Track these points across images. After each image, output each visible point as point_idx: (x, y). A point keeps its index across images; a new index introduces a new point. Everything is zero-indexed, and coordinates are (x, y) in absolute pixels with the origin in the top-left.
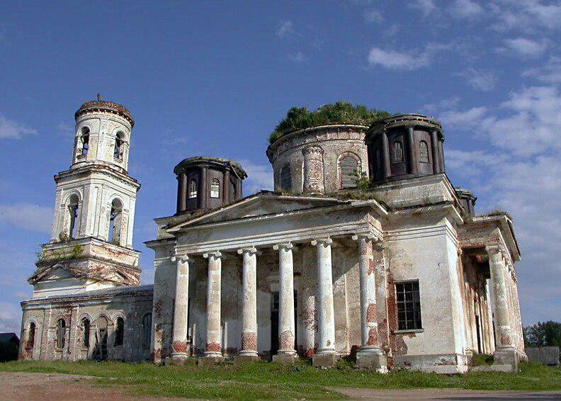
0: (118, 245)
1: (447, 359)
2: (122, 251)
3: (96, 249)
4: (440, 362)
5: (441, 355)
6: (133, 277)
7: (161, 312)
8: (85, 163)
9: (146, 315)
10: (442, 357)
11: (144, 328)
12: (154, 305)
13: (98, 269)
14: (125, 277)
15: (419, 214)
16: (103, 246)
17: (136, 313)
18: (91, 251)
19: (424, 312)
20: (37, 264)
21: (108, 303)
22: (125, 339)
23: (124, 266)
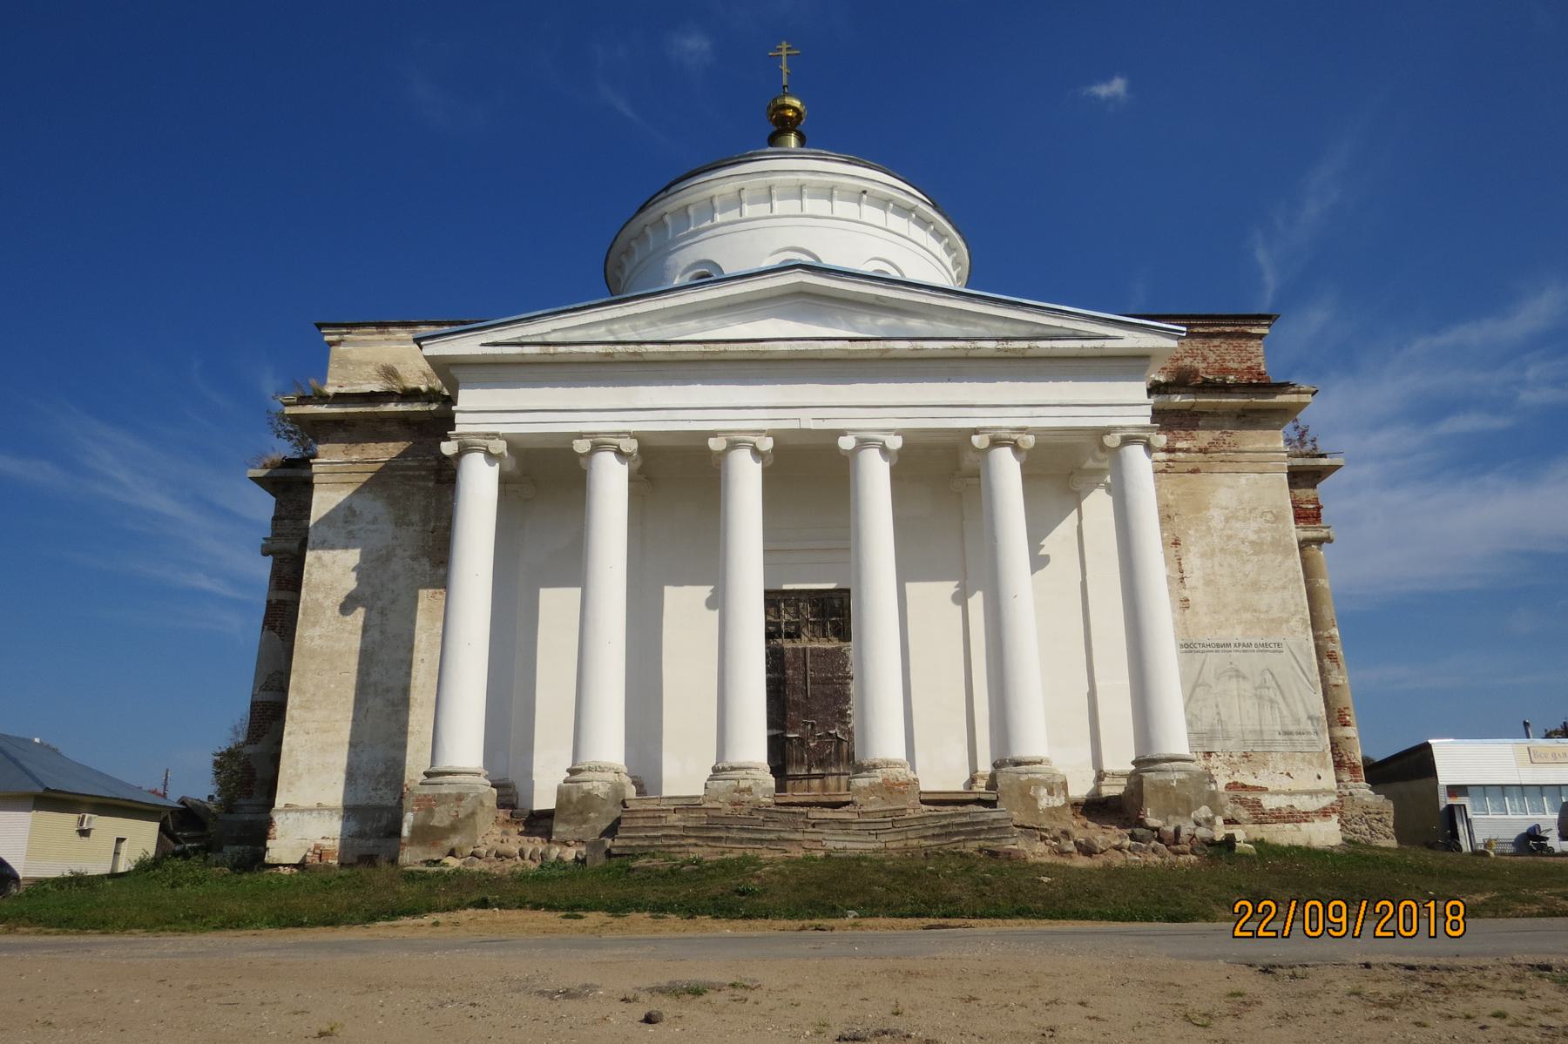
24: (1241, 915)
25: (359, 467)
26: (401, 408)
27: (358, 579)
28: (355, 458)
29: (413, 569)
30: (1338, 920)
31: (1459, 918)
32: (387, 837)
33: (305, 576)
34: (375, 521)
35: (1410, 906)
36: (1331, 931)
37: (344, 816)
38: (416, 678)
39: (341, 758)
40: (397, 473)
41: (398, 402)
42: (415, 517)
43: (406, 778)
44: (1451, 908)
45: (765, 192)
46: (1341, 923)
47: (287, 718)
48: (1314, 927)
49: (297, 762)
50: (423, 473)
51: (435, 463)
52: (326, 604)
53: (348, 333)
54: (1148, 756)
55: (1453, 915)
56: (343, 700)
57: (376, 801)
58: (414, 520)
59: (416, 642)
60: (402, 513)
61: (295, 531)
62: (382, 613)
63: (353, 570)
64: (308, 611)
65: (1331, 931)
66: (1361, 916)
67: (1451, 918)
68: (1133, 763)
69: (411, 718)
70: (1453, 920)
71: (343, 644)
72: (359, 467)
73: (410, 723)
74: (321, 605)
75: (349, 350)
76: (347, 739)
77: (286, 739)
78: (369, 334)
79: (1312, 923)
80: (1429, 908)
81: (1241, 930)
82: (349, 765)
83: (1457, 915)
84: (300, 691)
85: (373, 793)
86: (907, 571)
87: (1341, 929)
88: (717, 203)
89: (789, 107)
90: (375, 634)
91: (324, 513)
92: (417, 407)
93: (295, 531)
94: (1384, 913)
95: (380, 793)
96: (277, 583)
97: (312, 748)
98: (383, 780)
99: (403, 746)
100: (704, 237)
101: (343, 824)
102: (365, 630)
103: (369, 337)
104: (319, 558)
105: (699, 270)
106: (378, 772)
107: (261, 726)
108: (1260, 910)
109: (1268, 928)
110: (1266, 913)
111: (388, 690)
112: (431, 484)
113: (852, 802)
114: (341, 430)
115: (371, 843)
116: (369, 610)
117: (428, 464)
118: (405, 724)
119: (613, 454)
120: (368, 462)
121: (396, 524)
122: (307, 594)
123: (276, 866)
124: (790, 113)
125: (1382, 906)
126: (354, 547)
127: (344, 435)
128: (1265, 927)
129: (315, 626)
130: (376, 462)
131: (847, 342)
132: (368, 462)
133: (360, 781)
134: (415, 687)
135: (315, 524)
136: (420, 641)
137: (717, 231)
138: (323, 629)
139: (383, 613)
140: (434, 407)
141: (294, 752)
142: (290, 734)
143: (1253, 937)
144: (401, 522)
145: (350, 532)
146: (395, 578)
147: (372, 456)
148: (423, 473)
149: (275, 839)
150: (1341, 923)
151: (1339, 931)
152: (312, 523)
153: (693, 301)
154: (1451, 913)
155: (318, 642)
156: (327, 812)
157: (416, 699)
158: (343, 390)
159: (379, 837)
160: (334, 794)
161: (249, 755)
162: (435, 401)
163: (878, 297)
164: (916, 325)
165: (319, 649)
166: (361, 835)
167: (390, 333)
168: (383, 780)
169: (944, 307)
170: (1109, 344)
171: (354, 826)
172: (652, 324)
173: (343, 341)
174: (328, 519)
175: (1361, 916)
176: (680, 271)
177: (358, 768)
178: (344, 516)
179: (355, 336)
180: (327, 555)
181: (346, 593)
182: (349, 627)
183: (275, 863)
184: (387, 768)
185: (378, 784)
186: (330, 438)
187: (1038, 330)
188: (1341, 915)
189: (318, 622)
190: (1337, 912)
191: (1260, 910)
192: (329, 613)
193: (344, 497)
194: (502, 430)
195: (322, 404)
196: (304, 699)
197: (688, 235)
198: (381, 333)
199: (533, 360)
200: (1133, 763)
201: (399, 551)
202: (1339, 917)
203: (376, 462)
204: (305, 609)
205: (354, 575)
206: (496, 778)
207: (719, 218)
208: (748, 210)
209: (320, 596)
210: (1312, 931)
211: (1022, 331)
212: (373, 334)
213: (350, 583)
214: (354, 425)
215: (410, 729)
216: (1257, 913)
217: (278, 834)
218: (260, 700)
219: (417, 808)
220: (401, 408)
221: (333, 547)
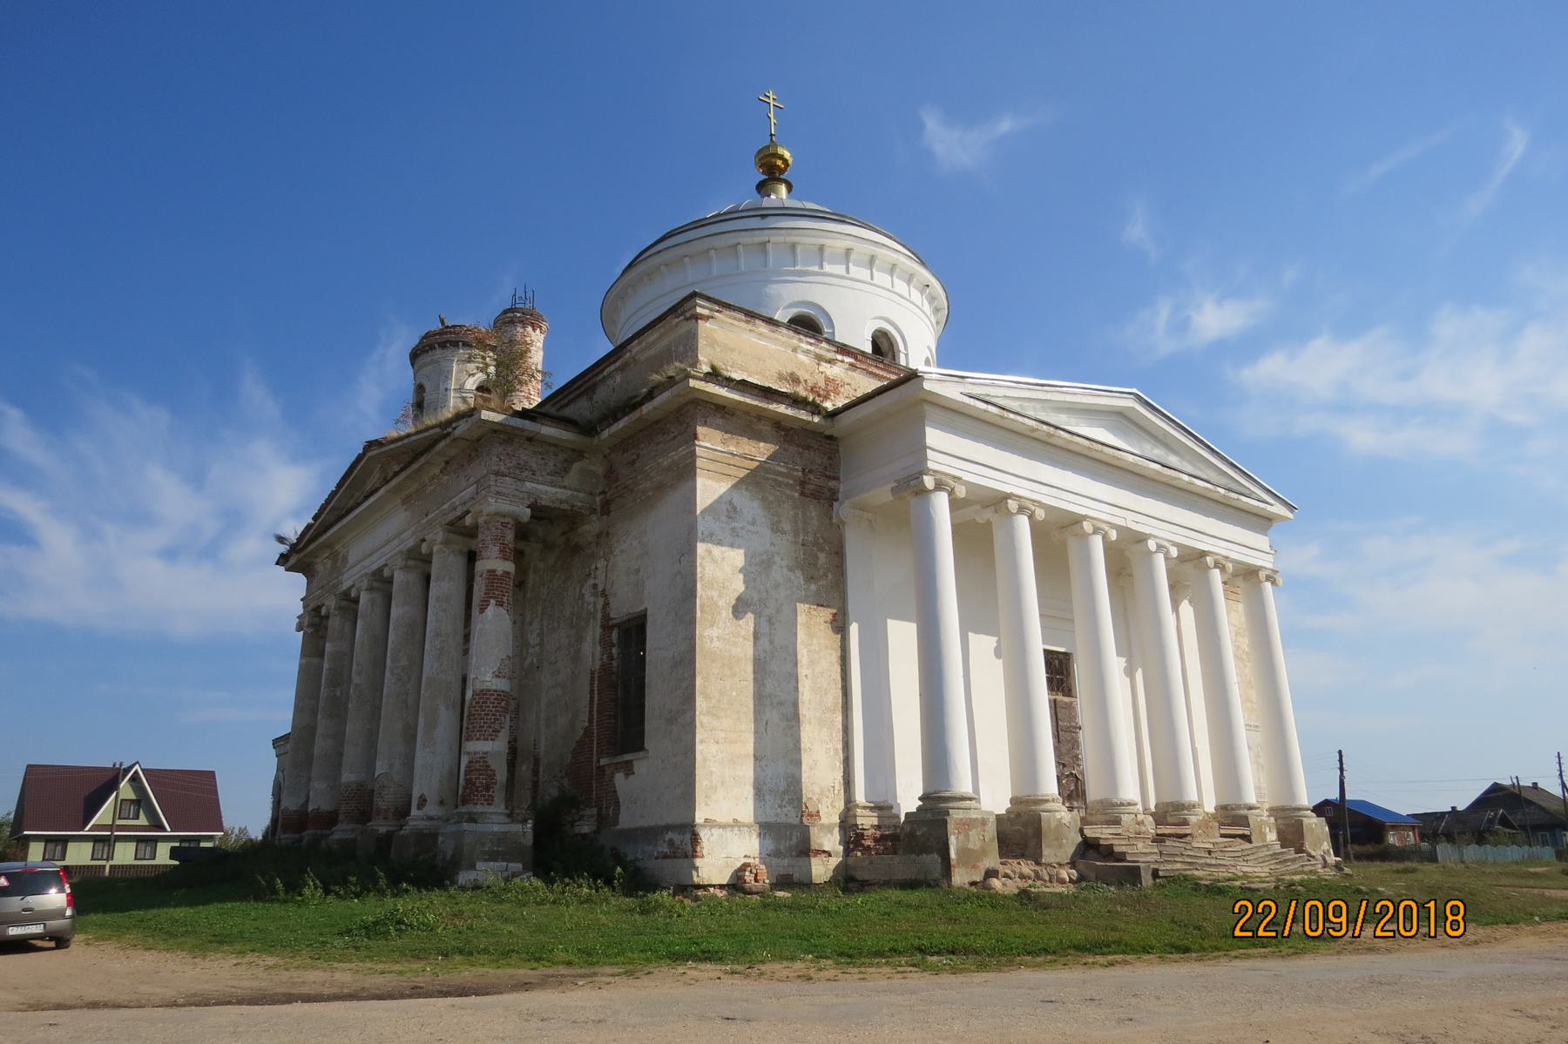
24: (1266, 914)
25: (737, 461)
26: (790, 412)
27: (745, 582)
28: (732, 449)
29: (790, 580)
30: (1338, 920)
31: (1459, 918)
32: (798, 856)
33: (699, 570)
34: (753, 523)
35: (1315, 906)
36: (1331, 931)
37: (760, 834)
38: (803, 694)
39: (747, 771)
40: (770, 476)
41: (789, 405)
42: (787, 526)
43: (804, 796)
44: (1451, 908)
45: (867, 259)
46: (1341, 923)
47: (697, 724)
48: (1314, 927)
49: (711, 773)
50: (791, 482)
51: (800, 474)
52: (720, 603)
53: (717, 311)
54: (1293, 806)
55: (1453, 915)
56: (745, 709)
57: (783, 819)
58: (786, 529)
59: (799, 657)
60: (776, 519)
61: (517, 493)
62: (770, 621)
63: (740, 571)
64: (705, 608)
65: (1331, 931)
66: (1360, 920)
67: (1451, 918)
68: (920, 799)
69: (802, 735)
70: (1453, 920)
71: (739, 650)
72: (737, 461)
73: (803, 740)
74: (716, 604)
75: (715, 329)
76: (750, 747)
77: (699, 747)
78: (735, 319)
79: (1312, 924)
80: (1429, 908)
81: (1382, 930)
82: (756, 779)
83: (1457, 915)
84: (707, 697)
85: (779, 811)
86: (966, 627)
87: (1341, 929)
88: (827, 253)
89: (781, 157)
90: (765, 642)
91: (709, 502)
92: (803, 415)
93: (517, 493)
94: (1243, 913)
95: (785, 810)
96: (501, 551)
97: (723, 759)
98: (786, 797)
99: (798, 763)
100: (811, 280)
101: (760, 842)
102: (756, 636)
103: (736, 323)
104: (710, 552)
105: (805, 310)
106: (781, 789)
107: (498, 719)
108: (1260, 910)
109: (1385, 929)
110: (1243, 913)
111: (781, 704)
112: (797, 495)
113: (1190, 834)
114: (719, 416)
115: (786, 861)
116: (758, 616)
117: (796, 473)
118: (797, 742)
119: (1027, 518)
120: (745, 458)
121: (772, 529)
122: (703, 589)
123: (705, 887)
124: (779, 163)
125: (1241, 906)
126: (739, 547)
127: (720, 421)
128: (1383, 927)
129: (713, 626)
130: (752, 460)
131: (1160, 466)
132: (745, 458)
133: (767, 797)
134: (803, 703)
135: (702, 512)
136: (803, 656)
137: (819, 279)
138: (720, 631)
139: (770, 621)
140: (816, 419)
141: (708, 762)
142: (702, 742)
143: (1253, 937)
144: (776, 528)
145: (733, 529)
146: (777, 586)
147: (746, 451)
148: (791, 482)
149: (703, 857)
150: (1341, 923)
151: (1339, 931)
152: (698, 512)
153: (1063, 400)
154: (1451, 913)
155: (716, 644)
156: (746, 829)
157: (805, 715)
158: (750, 380)
159: (792, 856)
160: (746, 810)
161: (486, 753)
162: (819, 414)
163: (1166, 433)
164: (1173, 460)
165: (718, 652)
166: (777, 854)
167: (754, 324)
168: (786, 797)
169: (1194, 450)
170: (1269, 508)
171: (770, 845)
172: (1044, 409)
173: (712, 317)
174: (710, 510)
175: (1360, 920)
176: (785, 304)
177: (765, 784)
178: (725, 509)
179: (724, 317)
180: (717, 551)
181: (736, 595)
182: (743, 633)
183: (706, 883)
184: (788, 785)
185: (782, 801)
186: (708, 420)
187: (1247, 492)
188: (1341, 915)
189: (714, 622)
190: (1455, 911)
191: (1260, 910)
192: (724, 612)
193: (725, 490)
194: (967, 477)
195: (724, 386)
196: (711, 705)
197: (791, 271)
198: (747, 322)
199: (992, 421)
200: (920, 799)
201: (777, 559)
202: (1339, 917)
203: (752, 460)
204: (702, 606)
205: (741, 576)
206: (878, 800)
207: (828, 268)
208: (855, 271)
209: (715, 594)
210: (1312, 931)
211: (1224, 481)
212: (740, 320)
213: (738, 586)
214: (733, 415)
215: (802, 746)
216: (1257, 913)
217: (705, 852)
218: (494, 687)
219: (956, 831)
220: (790, 412)
221: (720, 543)
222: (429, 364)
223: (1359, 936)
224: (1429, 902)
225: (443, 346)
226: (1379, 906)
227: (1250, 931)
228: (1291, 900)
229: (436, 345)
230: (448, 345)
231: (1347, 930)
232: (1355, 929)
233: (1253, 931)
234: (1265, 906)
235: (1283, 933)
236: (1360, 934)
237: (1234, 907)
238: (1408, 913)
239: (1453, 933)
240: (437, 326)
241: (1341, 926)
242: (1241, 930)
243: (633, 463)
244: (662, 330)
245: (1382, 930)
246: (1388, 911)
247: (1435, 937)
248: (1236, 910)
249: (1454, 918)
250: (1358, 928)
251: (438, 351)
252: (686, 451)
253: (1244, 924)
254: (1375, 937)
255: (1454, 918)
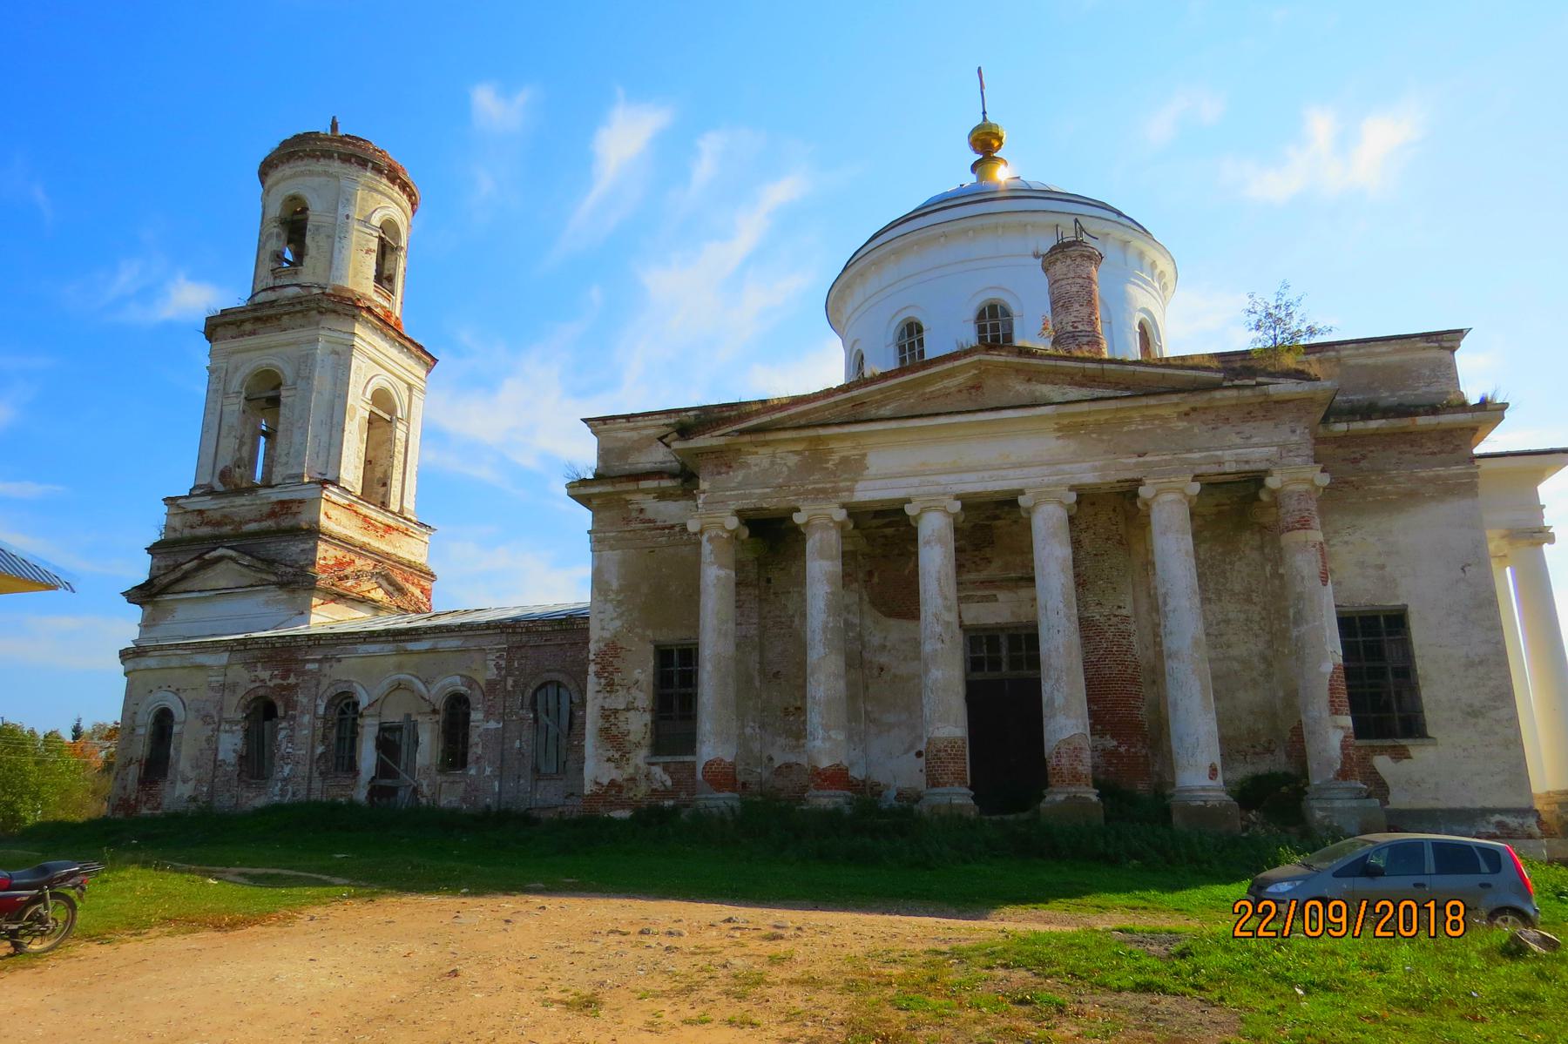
0: (384, 505)
1: (1512, 822)
2: (391, 522)
3: (334, 512)
4: (1492, 830)
5: (1493, 811)
6: (417, 592)
7: (617, 678)
8: (297, 289)
9: (543, 686)
10: (1497, 818)
11: (536, 720)
12: (592, 657)
13: (340, 564)
14: (401, 590)
15: (1127, 389)
16: (349, 508)
17: (510, 681)
18: (322, 517)
19: (1429, 716)
20: (800, 511)
21: (419, 652)
22: (475, 750)
23: (400, 563)
30: (1338, 920)
31: (1459, 918)
36: (1331, 931)
46: (1341, 923)
65: (1331, 931)
80: (1429, 908)
81: (1241, 930)
87: (1341, 929)
94: (1243, 913)
109: (1243, 929)
110: (1243, 913)
128: (1241, 927)
150: (1341, 923)
151: (1339, 931)
154: (1451, 913)
188: (1341, 915)
202: (1339, 917)
222: (319, 174)
223: (1288, 937)
224: (1429, 902)
225: (346, 159)
226: (1238, 906)
227: (1250, 931)
228: (1362, 900)
229: (336, 155)
230: (353, 160)
231: (1347, 931)
232: (1355, 929)
233: (1253, 931)
234: (1383, 906)
235: (1283, 933)
236: (1360, 935)
237: (1233, 908)
238: (1408, 911)
239: (1453, 933)
240: (324, 128)
241: (1341, 927)
242: (1382, 930)
243: (1355, 461)
244: (1397, 347)
245: (1241, 930)
246: (1388, 911)
247: (1435, 937)
248: (1236, 910)
249: (1454, 918)
250: (1358, 928)
251: (336, 166)
252: (1464, 471)
253: (1385, 924)
254: (1375, 937)
255: (1454, 918)
